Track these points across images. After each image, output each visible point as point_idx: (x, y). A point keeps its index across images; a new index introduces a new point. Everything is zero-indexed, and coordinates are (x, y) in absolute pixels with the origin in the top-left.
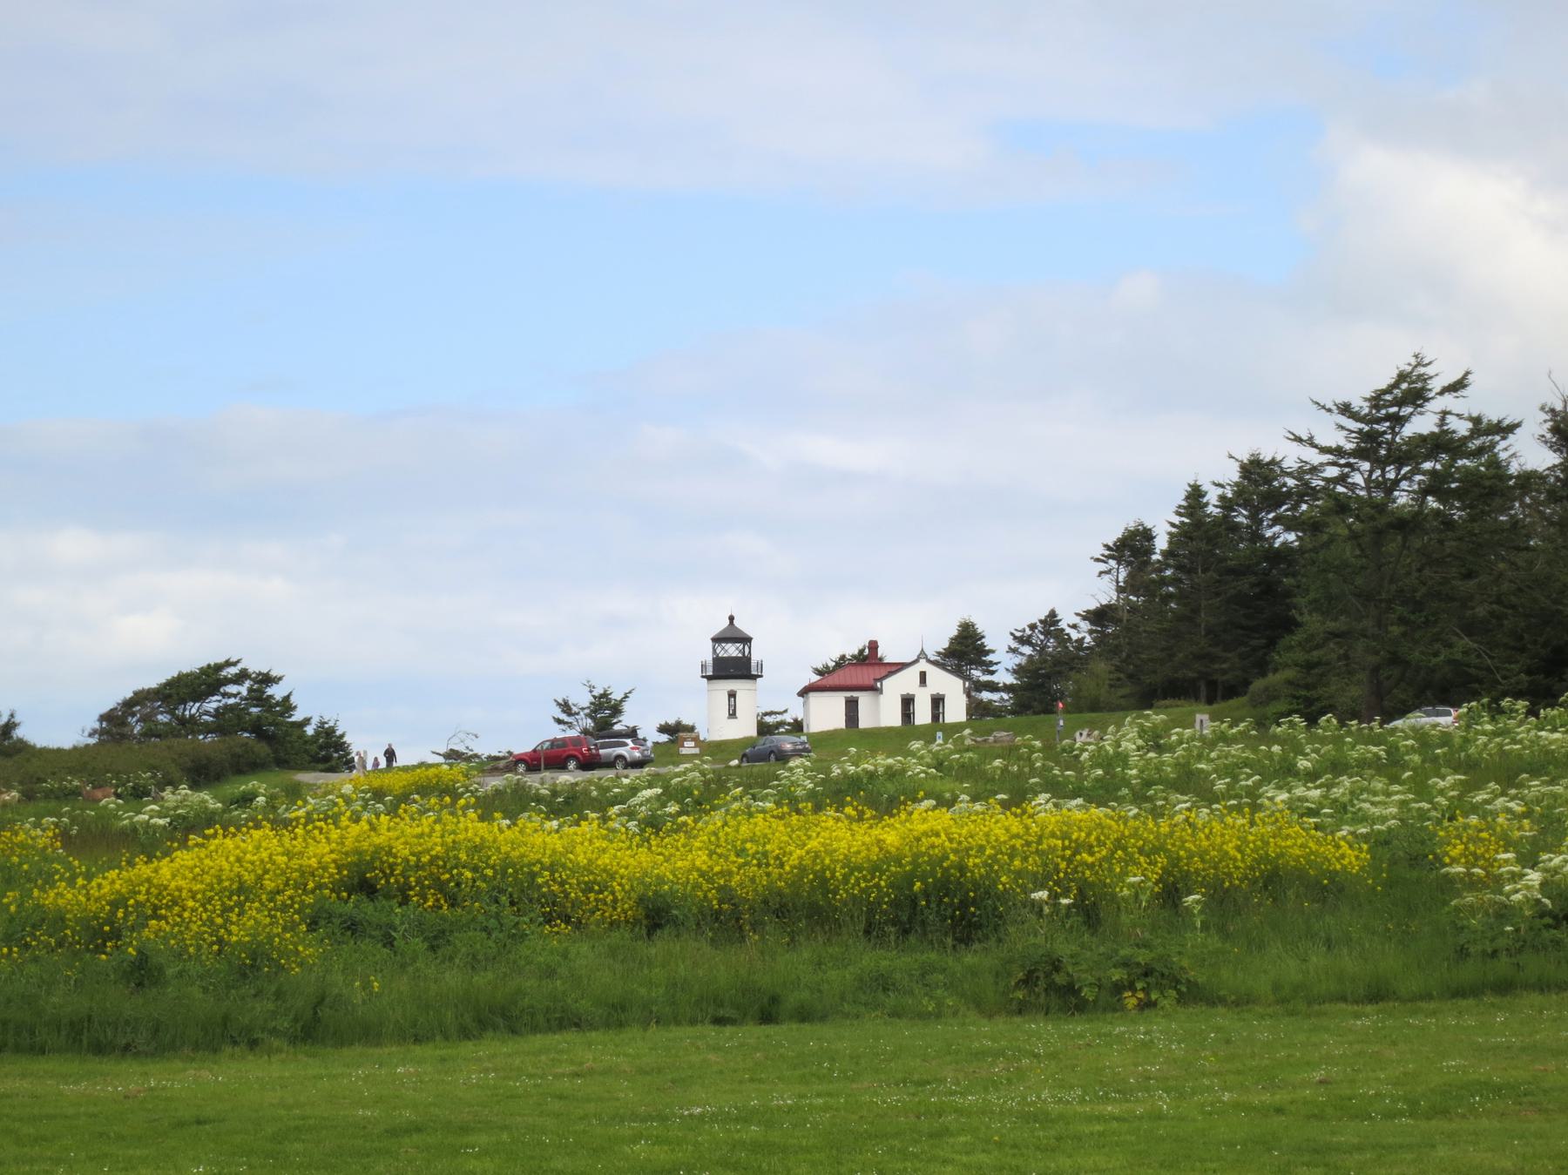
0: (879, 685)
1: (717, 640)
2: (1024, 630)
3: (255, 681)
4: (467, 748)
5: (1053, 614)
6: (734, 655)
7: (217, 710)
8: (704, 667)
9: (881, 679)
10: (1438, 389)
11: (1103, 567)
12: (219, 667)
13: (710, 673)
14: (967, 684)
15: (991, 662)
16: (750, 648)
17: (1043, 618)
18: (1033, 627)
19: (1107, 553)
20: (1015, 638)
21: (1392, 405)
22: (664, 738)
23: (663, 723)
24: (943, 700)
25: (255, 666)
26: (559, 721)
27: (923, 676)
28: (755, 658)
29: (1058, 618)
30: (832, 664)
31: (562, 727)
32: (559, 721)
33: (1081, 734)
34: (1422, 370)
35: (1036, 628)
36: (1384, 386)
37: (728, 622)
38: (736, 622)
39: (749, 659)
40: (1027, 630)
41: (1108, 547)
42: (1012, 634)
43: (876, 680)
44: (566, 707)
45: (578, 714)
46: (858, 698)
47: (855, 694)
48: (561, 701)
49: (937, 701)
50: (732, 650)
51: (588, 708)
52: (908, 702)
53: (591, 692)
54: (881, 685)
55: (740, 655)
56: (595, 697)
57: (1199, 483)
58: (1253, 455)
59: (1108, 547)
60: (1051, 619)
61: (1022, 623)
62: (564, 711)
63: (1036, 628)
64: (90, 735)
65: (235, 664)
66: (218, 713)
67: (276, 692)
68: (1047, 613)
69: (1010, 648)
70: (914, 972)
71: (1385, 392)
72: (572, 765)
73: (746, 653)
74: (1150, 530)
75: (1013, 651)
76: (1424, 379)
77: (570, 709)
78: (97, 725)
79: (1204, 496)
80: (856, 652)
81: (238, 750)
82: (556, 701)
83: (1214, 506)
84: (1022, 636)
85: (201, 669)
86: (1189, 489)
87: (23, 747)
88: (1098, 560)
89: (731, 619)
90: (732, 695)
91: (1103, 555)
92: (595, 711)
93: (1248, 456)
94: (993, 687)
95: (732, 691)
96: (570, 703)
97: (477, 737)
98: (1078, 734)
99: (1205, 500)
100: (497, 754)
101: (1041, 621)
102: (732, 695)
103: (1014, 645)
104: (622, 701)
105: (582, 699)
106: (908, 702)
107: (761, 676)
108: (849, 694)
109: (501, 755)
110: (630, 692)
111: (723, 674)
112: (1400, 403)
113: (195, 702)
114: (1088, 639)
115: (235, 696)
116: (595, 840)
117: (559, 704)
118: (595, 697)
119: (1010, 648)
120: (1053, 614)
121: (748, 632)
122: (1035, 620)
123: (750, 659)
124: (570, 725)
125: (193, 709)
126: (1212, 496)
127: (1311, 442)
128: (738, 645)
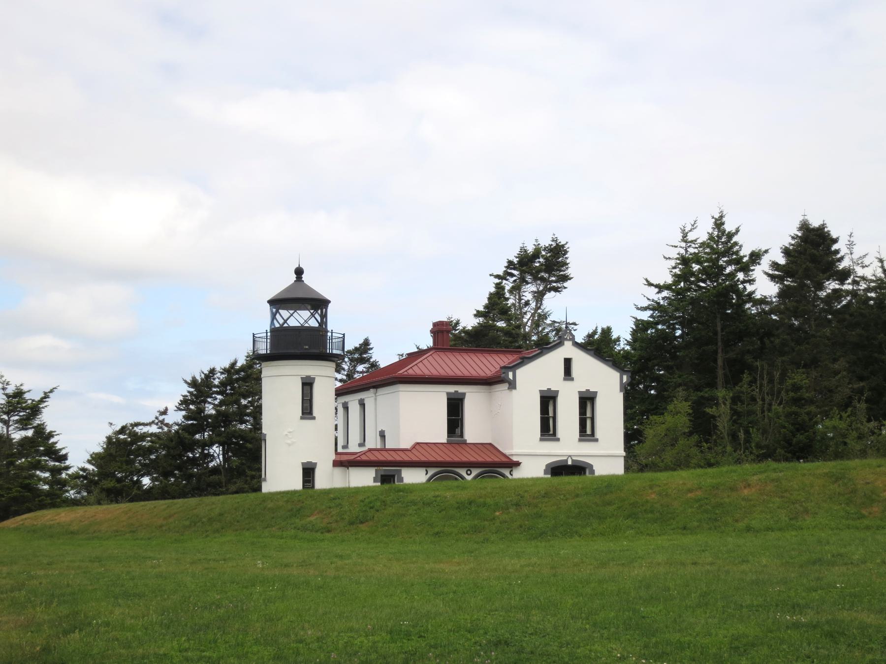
1: (277, 303)
9: (514, 368)
27: (568, 362)
37: (294, 277)
38: (305, 277)
43: (506, 368)
46: (464, 394)
47: (461, 389)
49: (587, 401)
50: (301, 318)
52: (548, 400)
53: (4, 389)
56: (8, 396)
70: (34, 639)
74: (563, 246)
89: (299, 272)
95: (308, 377)
102: (308, 385)
104: (42, 401)
106: (548, 400)
108: (452, 389)
110: (51, 391)
111: (297, 351)
114: (618, 348)
116: (123, 616)
118: (8, 396)
121: (325, 293)
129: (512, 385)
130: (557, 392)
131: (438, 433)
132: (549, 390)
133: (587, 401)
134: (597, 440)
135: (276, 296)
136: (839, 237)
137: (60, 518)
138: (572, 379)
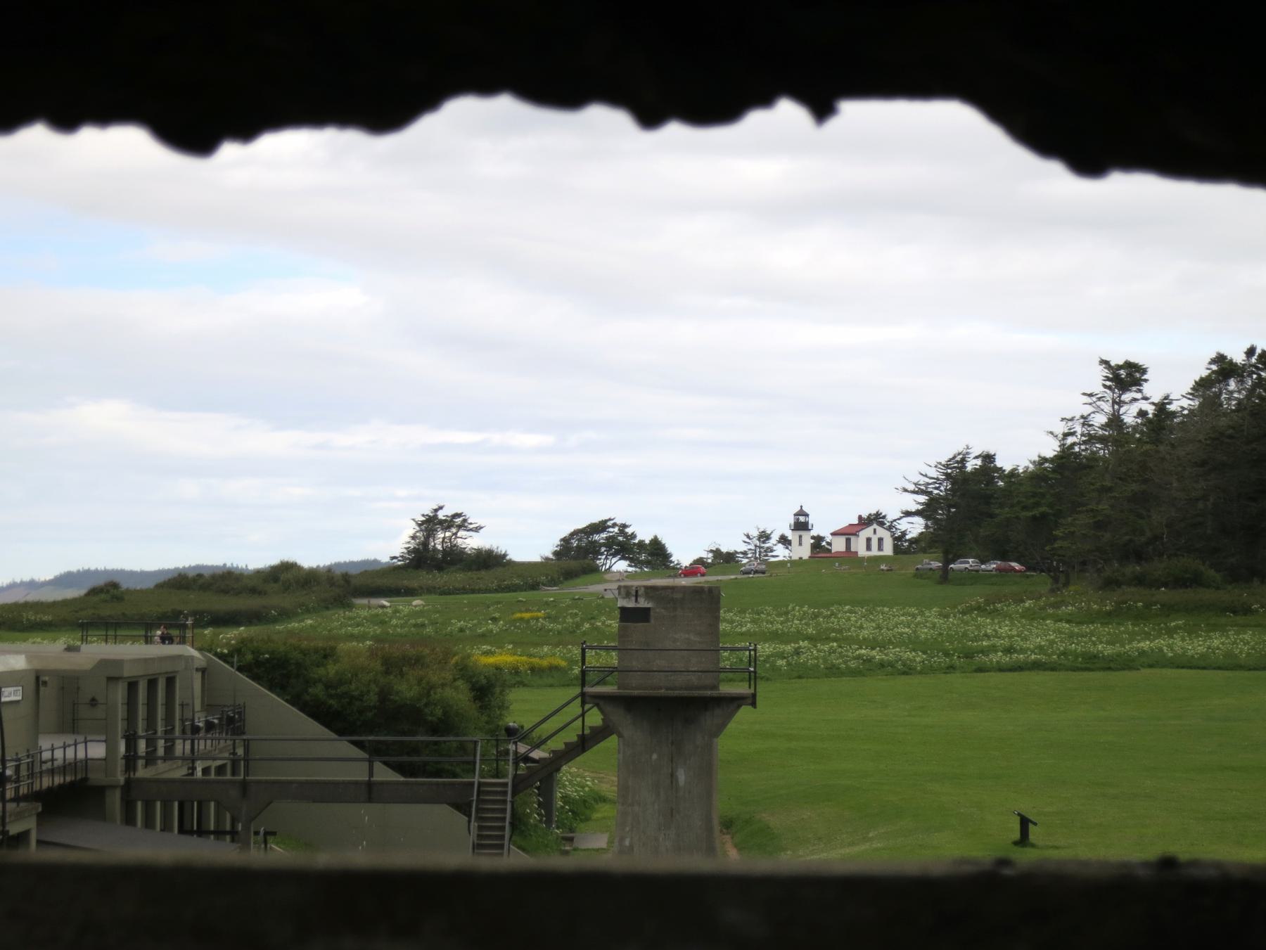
3: (620, 526)
7: (606, 537)
9: (859, 531)
12: (606, 521)
25: (619, 521)
26: (745, 542)
28: (810, 522)
32: (745, 542)
34: (968, 451)
39: (808, 523)
44: (748, 536)
49: (880, 540)
50: (802, 519)
52: (869, 540)
64: (557, 547)
65: (612, 520)
66: (607, 539)
67: (629, 531)
72: (699, 575)
78: (559, 543)
81: (585, 566)
85: (600, 522)
87: (511, 563)
89: (801, 507)
90: (800, 537)
92: (759, 538)
102: (800, 537)
105: (755, 533)
106: (869, 540)
108: (847, 536)
113: (597, 534)
115: (612, 532)
125: (596, 537)
127: (926, 476)
133: (880, 540)
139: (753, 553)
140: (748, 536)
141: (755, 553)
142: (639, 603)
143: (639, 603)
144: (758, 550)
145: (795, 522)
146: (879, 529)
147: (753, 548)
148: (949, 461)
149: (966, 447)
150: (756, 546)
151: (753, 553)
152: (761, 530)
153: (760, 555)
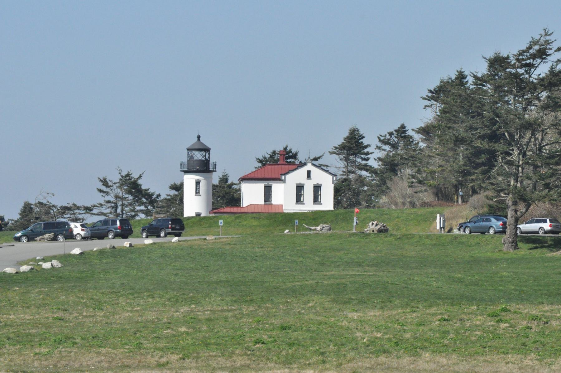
0: (283, 177)
2: (386, 135)
4: (48, 202)
5: (403, 127)
6: (200, 158)
8: (182, 165)
9: (285, 174)
10: (555, 48)
11: (427, 103)
13: (186, 169)
14: (335, 178)
15: (368, 152)
16: (209, 154)
17: (397, 128)
18: (391, 134)
19: (430, 95)
20: (380, 140)
21: (529, 59)
22: (173, 192)
23: (173, 183)
24: (320, 187)
26: (101, 191)
27: (309, 173)
28: (212, 161)
29: (406, 129)
30: (268, 156)
31: (102, 194)
32: (101, 191)
33: (373, 224)
34: (548, 38)
35: (393, 134)
36: (524, 48)
37: (196, 139)
38: (201, 139)
40: (388, 135)
41: (430, 91)
42: (379, 138)
44: (105, 182)
45: (112, 186)
47: (270, 183)
48: (102, 179)
49: (317, 188)
51: (119, 183)
52: (300, 188)
53: (120, 173)
54: (285, 178)
55: (203, 159)
57: (463, 70)
58: (496, 54)
59: (430, 91)
60: (402, 130)
61: (384, 131)
62: (104, 185)
63: (393, 134)
68: (399, 126)
69: (377, 146)
71: (524, 52)
73: (207, 157)
75: (379, 148)
76: (547, 43)
77: (107, 183)
79: (466, 78)
80: (282, 149)
82: (99, 179)
83: (341, 175)
84: (385, 139)
86: (457, 74)
88: (425, 99)
89: (199, 137)
91: (427, 96)
93: (493, 54)
94: (366, 168)
96: (108, 180)
97: (54, 195)
98: (371, 223)
99: (466, 80)
100: (67, 205)
101: (396, 131)
102: (198, 183)
103: (379, 144)
104: (138, 179)
105: (114, 178)
106: (300, 188)
107: (215, 171)
108: (266, 183)
109: (68, 206)
112: (534, 57)
117: (101, 181)
118: (122, 177)
119: (377, 146)
120: (403, 127)
121: (209, 145)
122: (392, 130)
123: (209, 161)
124: (107, 193)
126: (470, 80)
128: (202, 152)
129: (284, 181)
130: (304, 184)
131: (260, 201)
132: (318, 184)
133: (317, 188)
134: (304, 204)
135: (192, 145)
136: (97, 189)
137: (437, 310)
138: (311, 179)
139: (112, 207)
140: (105, 182)
141: (116, 207)
142: (302, 203)
143: (302, 203)
144: (120, 203)
145: (188, 161)
146: (315, 172)
147: (112, 199)
148: (520, 54)
149: (543, 34)
150: (117, 197)
151: (112, 207)
152: (124, 173)
153: (122, 211)
